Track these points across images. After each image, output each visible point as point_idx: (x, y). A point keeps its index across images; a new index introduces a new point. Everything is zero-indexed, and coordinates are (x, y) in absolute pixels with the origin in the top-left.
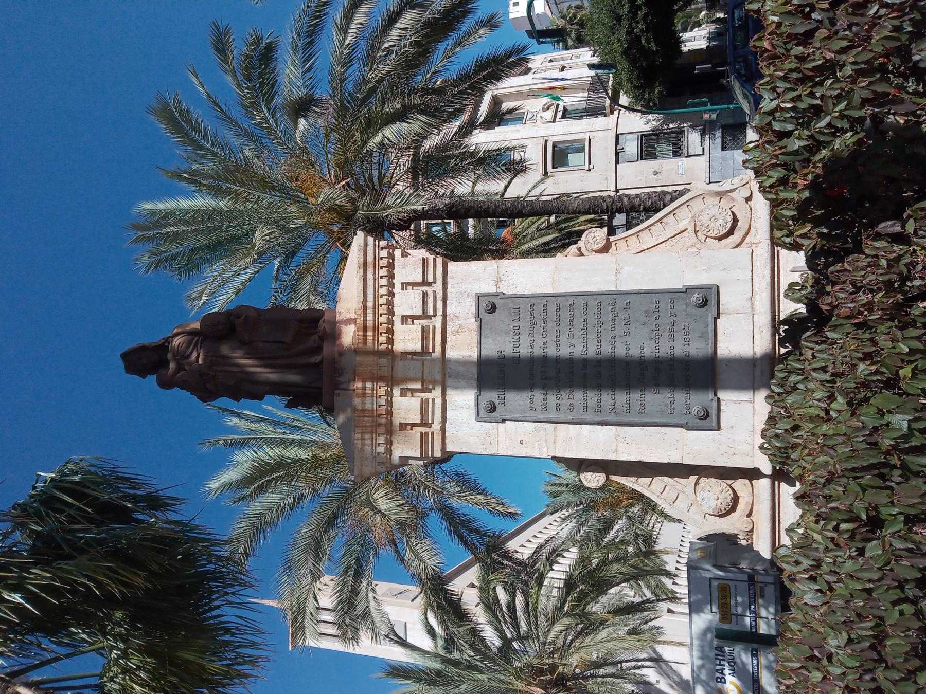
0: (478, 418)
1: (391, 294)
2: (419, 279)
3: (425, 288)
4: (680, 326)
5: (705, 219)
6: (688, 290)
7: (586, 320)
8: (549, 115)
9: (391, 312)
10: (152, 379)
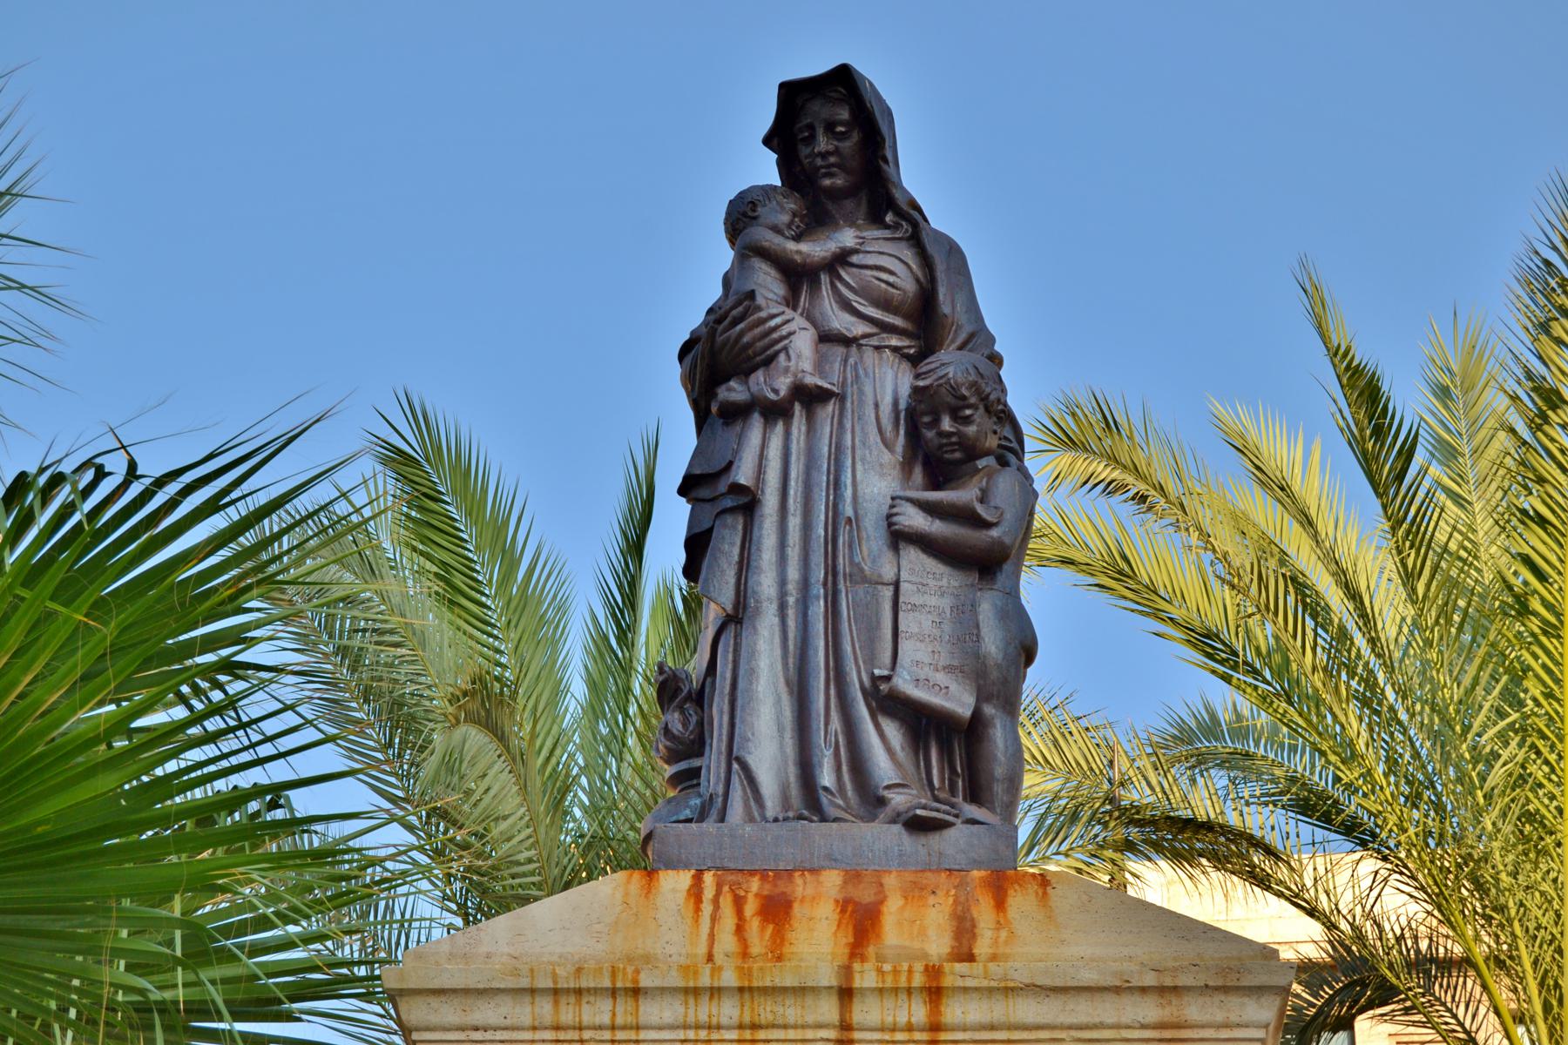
10: (766, 170)
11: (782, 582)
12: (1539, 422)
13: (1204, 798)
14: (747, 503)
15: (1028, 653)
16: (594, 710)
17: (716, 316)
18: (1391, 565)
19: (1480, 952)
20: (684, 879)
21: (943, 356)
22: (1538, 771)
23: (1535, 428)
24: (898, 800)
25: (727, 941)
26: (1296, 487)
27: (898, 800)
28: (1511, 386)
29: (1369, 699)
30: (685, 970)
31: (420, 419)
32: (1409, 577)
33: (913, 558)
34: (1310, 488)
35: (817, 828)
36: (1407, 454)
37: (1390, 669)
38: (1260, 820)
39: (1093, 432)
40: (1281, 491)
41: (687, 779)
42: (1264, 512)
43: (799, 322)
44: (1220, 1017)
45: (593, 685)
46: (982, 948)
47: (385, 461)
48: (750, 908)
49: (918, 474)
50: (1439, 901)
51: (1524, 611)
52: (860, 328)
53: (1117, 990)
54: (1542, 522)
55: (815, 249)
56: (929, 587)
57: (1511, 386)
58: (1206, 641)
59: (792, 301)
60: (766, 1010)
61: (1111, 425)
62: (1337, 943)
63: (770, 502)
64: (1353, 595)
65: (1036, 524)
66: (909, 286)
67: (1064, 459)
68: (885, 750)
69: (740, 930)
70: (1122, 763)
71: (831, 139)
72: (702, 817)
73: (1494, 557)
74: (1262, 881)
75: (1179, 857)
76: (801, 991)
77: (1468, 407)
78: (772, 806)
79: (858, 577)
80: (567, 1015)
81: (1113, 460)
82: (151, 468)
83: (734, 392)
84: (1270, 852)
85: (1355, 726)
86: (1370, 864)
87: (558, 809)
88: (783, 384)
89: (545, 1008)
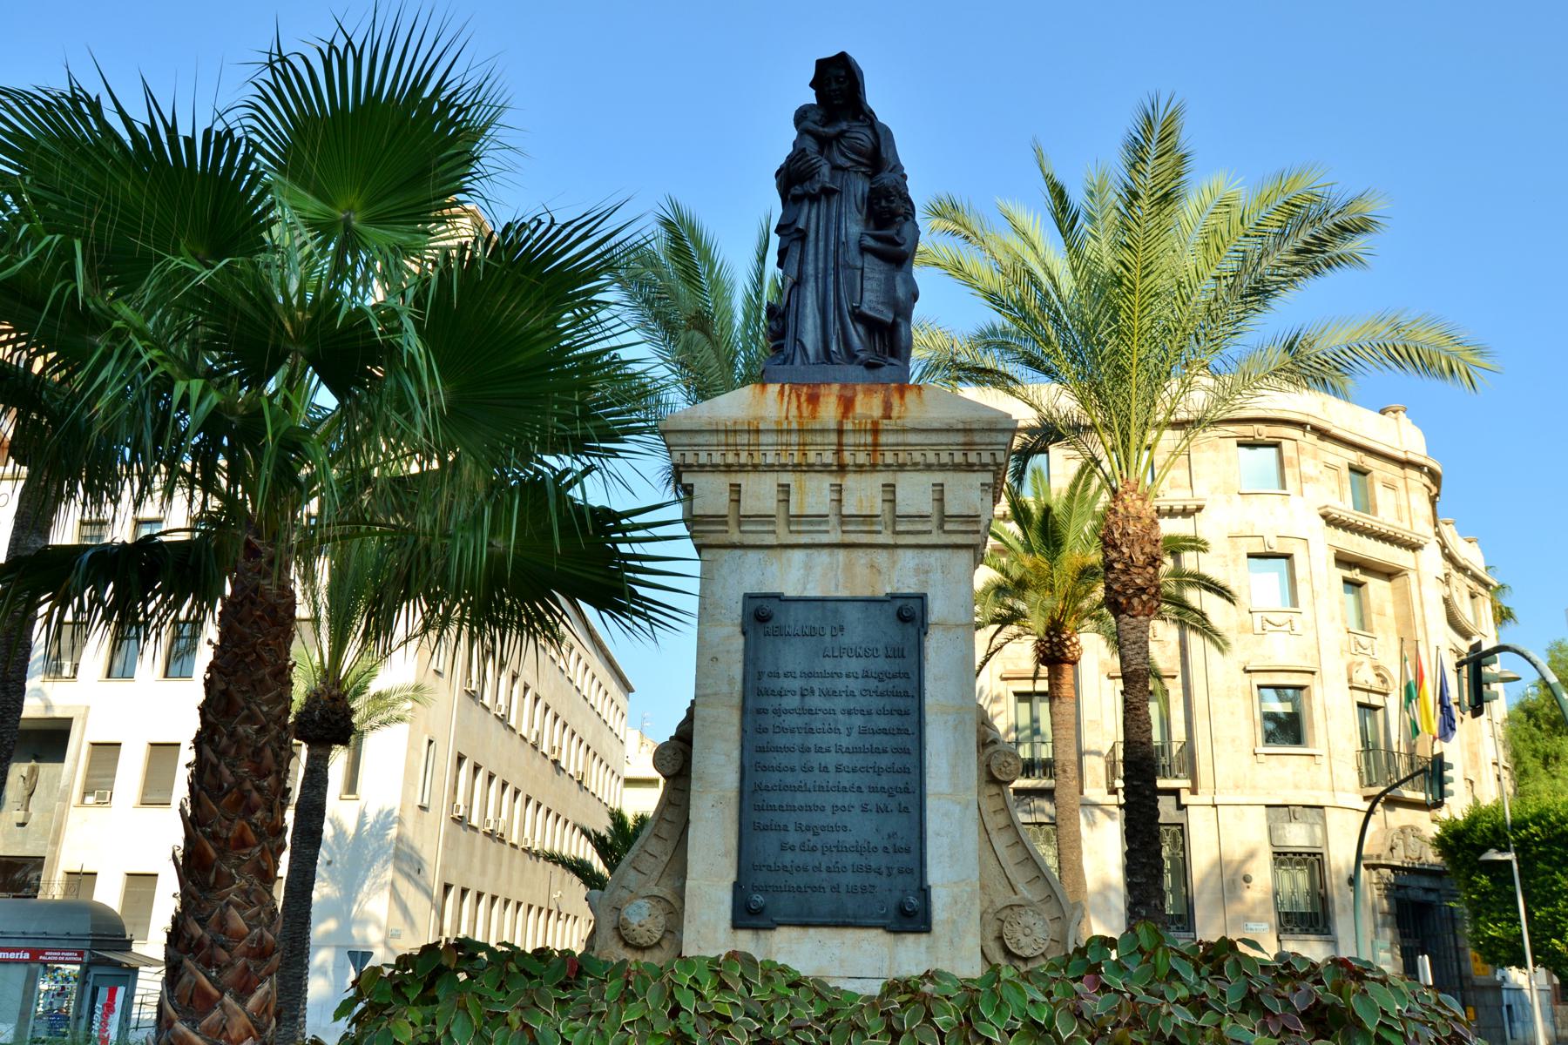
0: (749, 597)
1: (929, 467)
2: (949, 510)
3: (935, 519)
4: (873, 879)
5: (1029, 918)
6: (924, 892)
7: (885, 751)
8: (1366, 677)
9: (901, 467)
10: (810, 97)
11: (816, 268)
12: (1130, 205)
13: (989, 360)
14: (802, 236)
15: (915, 297)
16: (746, 325)
17: (790, 159)
18: (1067, 266)
19: (1098, 421)
20: (777, 387)
21: (882, 175)
22: (1123, 349)
23: (1128, 208)
24: (862, 356)
25: (794, 412)
26: (1030, 233)
27: (862, 356)
28: (1119, 190)
29: (1057, 320)
30: (777, 423)
31: (676, 207)
32: (1074, 270)
33: (869, 258)
34: (1036, 234)
35: (830, 367)
36: (1075, 219)
37: (1065, 307)
38: (1011, 369)
39: (947, 210)
40: (1024, 235)
41: (778, 349)
42: (1017, 244)
43: (824, 161)
44: (988, 441)
45: (746, 316)
46: (894, 414)
47: (662, 224)
48: (803, 399)
49: (872, 224)
50: (1082, 401)
51: (1120, 283)
52: (849, 164)
53: (948, 430)
54: (1129, 247)
55: (830, 130)
56: (874, 270)
57: (1119, 190)
58: (992, 297)
59: (821, 152)
60: (809, 438)
61: (955, 207)
62: (1042, 419)
63: (812, 236)
64: (1052, 278)
65: (920, 248)
66: (869, 145)
67: (936, 221)
68: (857, 336)
69: (799, 407)
70: (957, 346)
71: (838, 82)
72: (784, 363)
73: (1109, 262)
74: (1012, 393)
75: (979, 383)
76: (823, 431)
77: (1101, 199)
78: (812, 358)
79: (847, 266)
80: (731, 440)
81: (955, 221)
82: (560, 221)
83: (797, 190)
84: (1015, 381)
85: (1051, 332)
86: (1055, 386)
87: (732, 365)
88: (817, 187)
89: (722, 438)
